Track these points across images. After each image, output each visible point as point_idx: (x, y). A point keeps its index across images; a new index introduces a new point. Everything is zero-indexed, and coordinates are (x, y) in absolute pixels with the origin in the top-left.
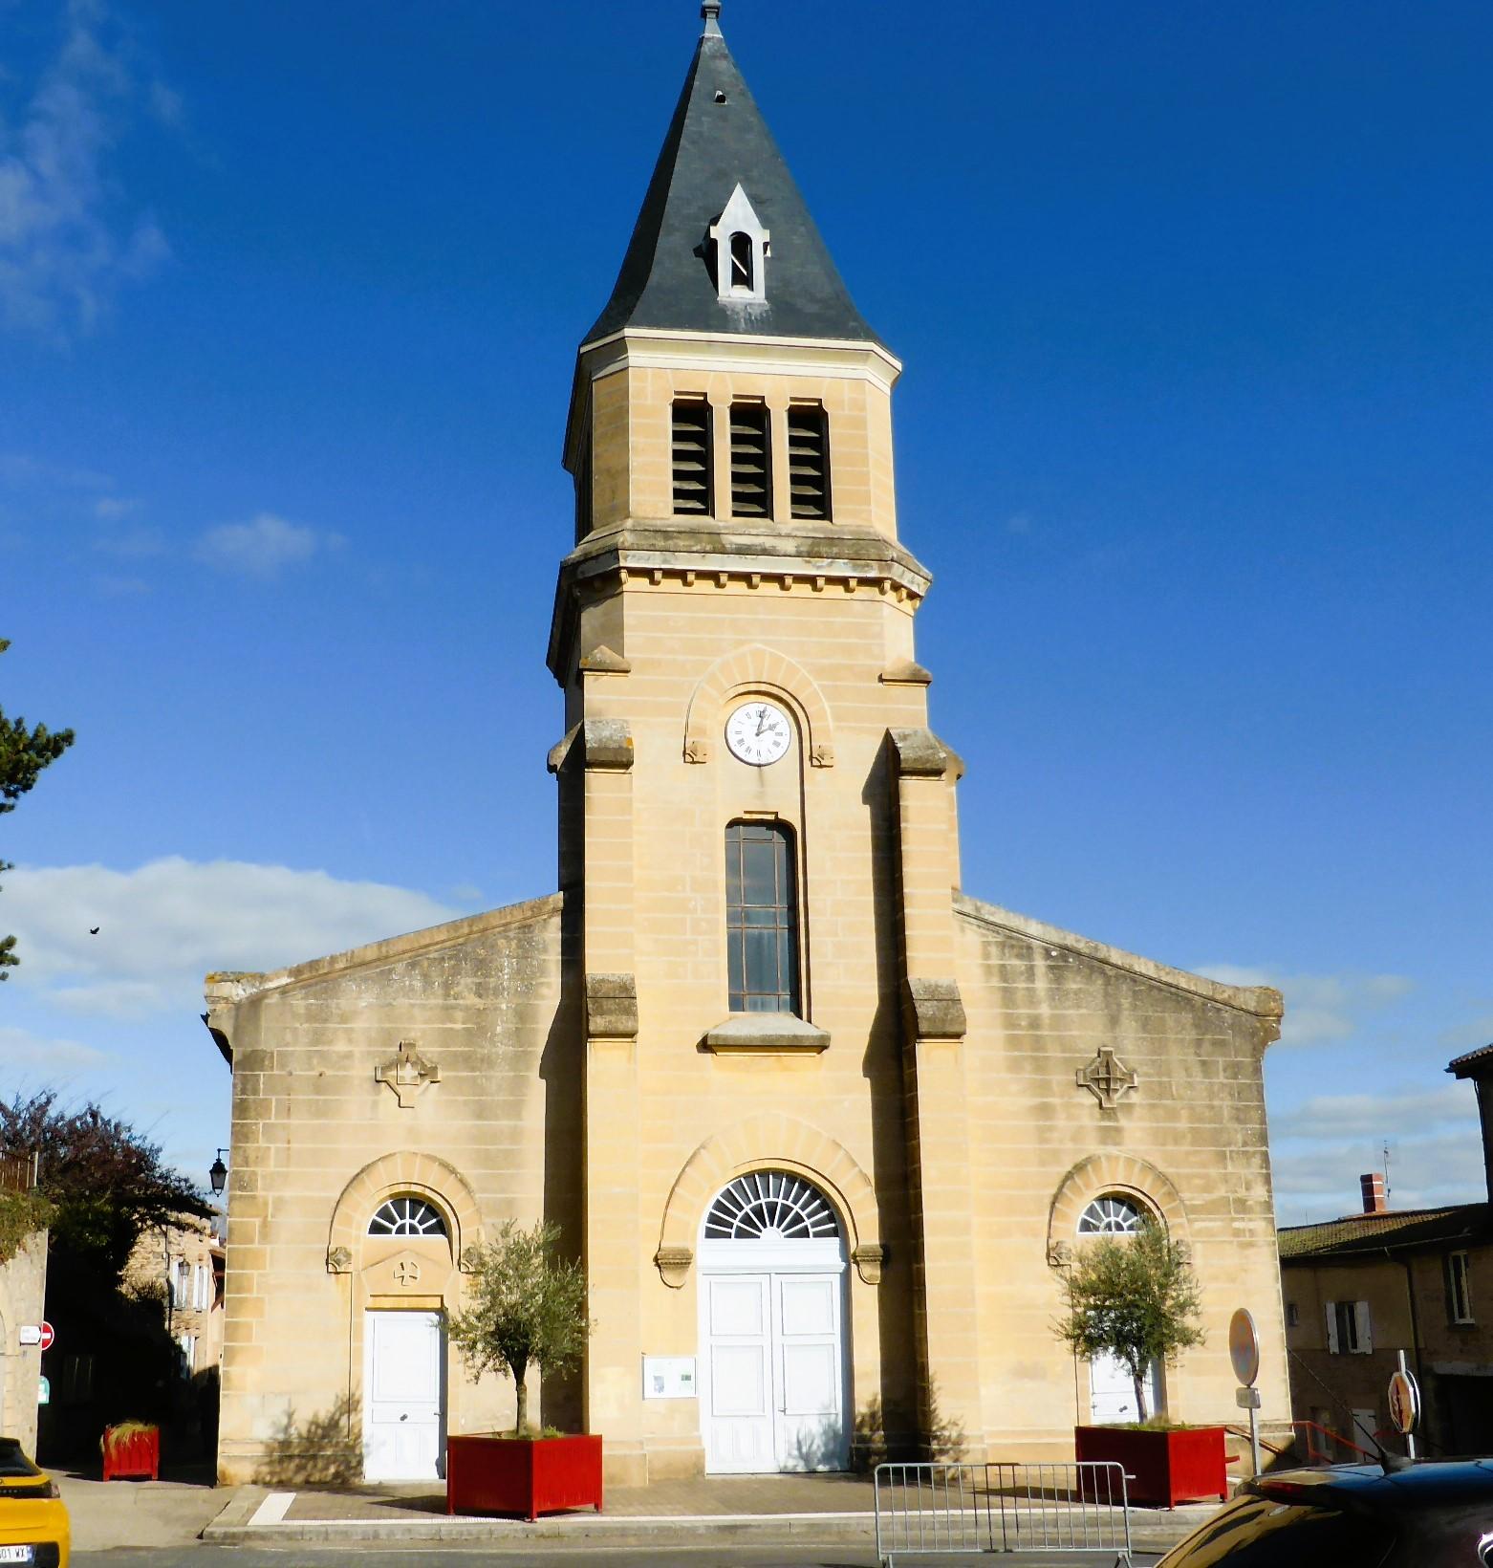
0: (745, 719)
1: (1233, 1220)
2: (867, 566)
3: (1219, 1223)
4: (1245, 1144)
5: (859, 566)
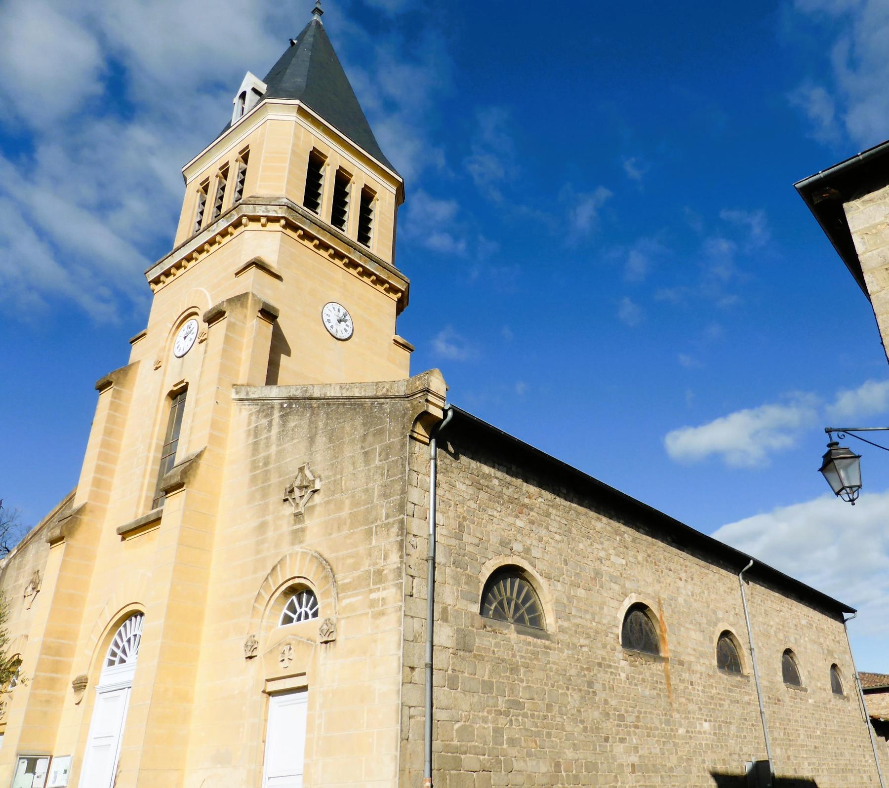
0: (332, 310)
1: (371, 591)
2: (231, 216)
3: (360, 598)
4: (387, 517)
5: (228, 218)
